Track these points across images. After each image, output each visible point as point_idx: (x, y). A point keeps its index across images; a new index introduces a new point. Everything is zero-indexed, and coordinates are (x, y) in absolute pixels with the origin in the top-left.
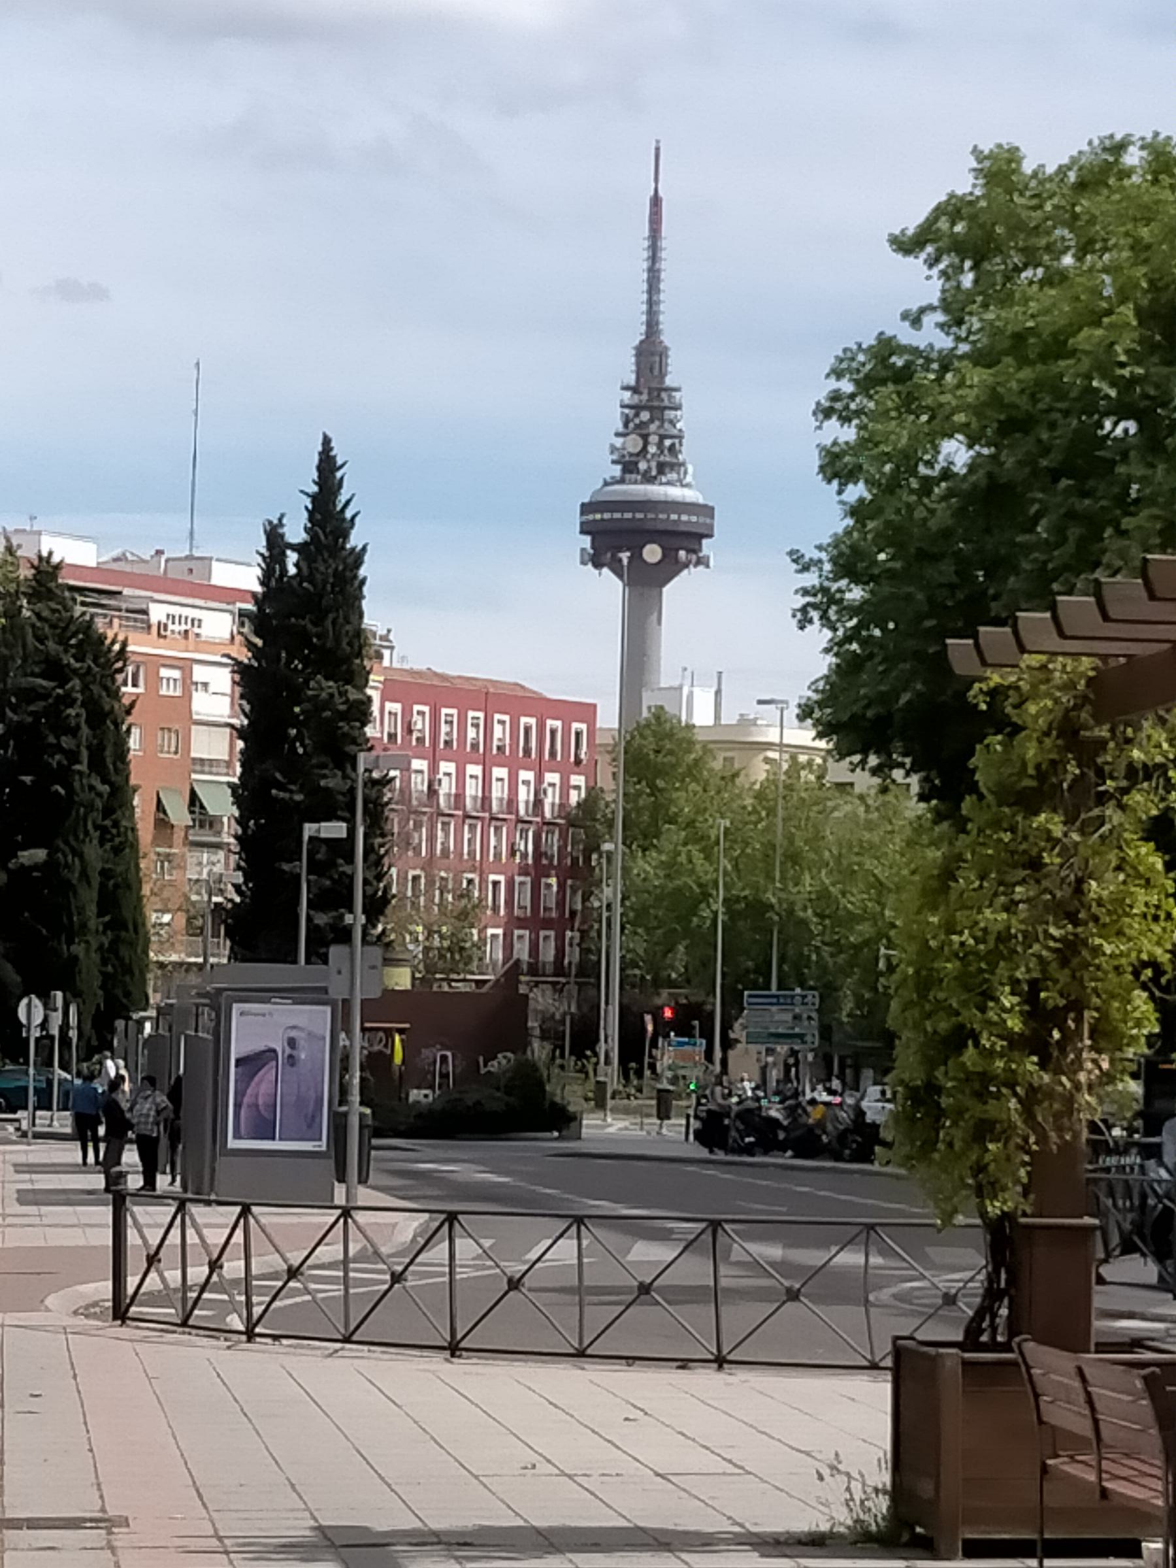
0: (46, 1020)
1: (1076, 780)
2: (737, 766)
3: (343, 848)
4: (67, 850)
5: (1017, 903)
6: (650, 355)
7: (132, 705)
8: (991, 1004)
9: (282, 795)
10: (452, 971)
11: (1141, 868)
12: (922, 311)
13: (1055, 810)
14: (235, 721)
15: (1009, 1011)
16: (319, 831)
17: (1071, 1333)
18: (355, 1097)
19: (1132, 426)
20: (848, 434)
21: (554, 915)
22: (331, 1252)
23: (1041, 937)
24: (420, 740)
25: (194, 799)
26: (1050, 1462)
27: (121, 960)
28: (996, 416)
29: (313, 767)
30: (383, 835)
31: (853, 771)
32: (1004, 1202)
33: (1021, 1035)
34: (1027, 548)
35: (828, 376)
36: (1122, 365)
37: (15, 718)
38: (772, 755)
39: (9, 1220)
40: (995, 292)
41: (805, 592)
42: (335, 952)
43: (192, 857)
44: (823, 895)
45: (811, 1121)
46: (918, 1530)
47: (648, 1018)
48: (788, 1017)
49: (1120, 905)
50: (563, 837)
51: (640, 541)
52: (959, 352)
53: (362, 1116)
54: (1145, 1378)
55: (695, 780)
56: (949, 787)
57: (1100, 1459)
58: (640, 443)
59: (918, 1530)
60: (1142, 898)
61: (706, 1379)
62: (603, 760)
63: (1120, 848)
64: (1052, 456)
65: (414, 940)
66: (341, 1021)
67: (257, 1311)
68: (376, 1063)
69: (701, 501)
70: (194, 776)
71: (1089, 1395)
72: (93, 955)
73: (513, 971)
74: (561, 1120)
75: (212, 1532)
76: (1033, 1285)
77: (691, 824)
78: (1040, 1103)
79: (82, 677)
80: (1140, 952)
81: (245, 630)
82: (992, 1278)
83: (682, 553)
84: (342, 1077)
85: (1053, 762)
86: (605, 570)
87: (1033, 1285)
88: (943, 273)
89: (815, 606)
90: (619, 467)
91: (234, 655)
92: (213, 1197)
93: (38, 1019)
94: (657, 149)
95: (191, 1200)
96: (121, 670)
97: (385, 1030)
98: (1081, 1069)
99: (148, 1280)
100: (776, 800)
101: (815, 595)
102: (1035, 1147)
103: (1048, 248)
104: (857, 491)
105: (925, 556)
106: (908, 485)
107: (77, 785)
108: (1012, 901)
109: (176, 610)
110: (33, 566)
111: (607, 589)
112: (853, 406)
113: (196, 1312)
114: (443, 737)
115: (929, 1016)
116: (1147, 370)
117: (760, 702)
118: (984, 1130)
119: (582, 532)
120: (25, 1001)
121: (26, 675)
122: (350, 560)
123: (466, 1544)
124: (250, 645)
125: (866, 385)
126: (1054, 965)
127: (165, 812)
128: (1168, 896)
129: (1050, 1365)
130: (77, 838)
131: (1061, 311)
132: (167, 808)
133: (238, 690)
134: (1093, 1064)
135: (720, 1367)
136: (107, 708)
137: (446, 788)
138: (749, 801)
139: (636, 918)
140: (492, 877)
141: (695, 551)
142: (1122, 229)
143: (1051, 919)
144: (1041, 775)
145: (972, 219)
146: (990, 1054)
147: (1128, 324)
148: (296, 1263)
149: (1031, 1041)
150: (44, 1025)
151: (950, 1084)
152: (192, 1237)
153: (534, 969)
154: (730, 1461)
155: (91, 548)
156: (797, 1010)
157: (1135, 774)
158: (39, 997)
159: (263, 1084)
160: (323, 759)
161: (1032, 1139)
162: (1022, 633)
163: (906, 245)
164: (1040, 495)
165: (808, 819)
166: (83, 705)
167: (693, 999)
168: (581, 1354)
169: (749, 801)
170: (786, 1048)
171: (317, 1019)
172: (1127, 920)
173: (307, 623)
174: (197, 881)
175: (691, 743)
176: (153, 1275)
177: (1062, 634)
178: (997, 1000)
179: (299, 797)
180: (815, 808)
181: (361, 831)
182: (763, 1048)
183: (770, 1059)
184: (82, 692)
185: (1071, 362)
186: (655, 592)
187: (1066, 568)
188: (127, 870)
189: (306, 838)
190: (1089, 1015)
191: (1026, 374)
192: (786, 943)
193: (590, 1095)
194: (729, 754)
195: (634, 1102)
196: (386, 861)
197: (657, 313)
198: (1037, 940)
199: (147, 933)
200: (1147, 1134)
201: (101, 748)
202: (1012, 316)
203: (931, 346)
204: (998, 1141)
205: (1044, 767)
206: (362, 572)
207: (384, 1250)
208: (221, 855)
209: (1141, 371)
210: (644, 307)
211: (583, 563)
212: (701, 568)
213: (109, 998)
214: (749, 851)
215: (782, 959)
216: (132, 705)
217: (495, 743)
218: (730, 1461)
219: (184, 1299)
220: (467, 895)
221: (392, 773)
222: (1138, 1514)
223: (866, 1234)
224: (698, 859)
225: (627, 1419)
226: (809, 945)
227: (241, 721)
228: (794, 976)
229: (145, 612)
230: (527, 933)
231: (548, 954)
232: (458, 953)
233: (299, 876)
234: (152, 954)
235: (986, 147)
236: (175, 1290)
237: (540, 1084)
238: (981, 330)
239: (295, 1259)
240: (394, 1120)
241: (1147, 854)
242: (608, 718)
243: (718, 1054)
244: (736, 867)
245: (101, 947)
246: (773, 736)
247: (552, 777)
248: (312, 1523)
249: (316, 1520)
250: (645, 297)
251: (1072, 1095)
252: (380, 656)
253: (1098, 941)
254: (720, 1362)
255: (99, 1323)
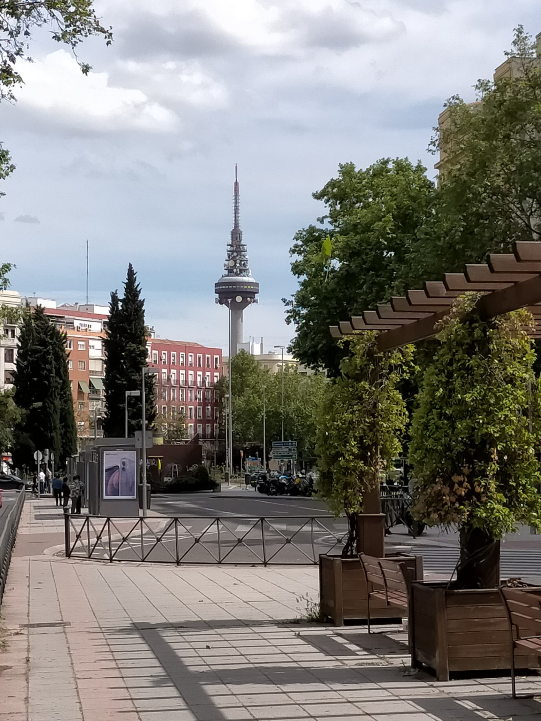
0: (43, 458)
1: (373, 370)
2: (268, 368)
3: (139, 399)
4: (49, 402)
5: (355, 411)
6: (236, 234)
7: (69, 354)
8: (348, 444)
9: (119, 382)
10: (177, 438)
11: (395, 398)
12: (324, 218)
13: (366, 381)
14: (103, 358)
15: (353, 447)
16: (131, 393)
17: (377, 552)
18: (145, 481)
19: (393, 253)
20: (300, 258)
21: (210, 419)
22: (137, 532)
23: (363, 422)
24: (164, 363)
25: (91, 384)
26: (371, 593)
27: (68, 438)
28: (348, 251)
29: (129, 372)
30: (153, 394)
31: (305, 368)
32: (355, 508)
33: (357, 454)
34: (359, 295)
35: (293, 239)
36: (389, 234)
37: (31, 359)
38: (280, 364)
39: (32, 525)
40: (347, 211)
41: (288, 312)
42: (137, 433)
43: (91, 403)
44: (298, 409)
45: (295, 483)
46: (329, 617)
47: (241, 451)
48: (287, 449)
49: (388, 411)
50: (212, 393)
51: (234, 295)
52: (336, 231)
53: (147, 487)
54: (400, 565)
55: (255, 372)
56: (334, 373)
57: (387, 591)
58: (234, 263)
59: (329, 617)
60: (395, 408)
61: (260, 570)
62: (225, 367)
63: (388, 392)
64: (367, 264)
65: (164, 428)
66: (140, 456)
67: (113, 552)
68: (152, 469)
69: (254, 281)
70: (90, 377)
71: (382, 571)
72: (58, 436)
73: (197, 437)
74: (214, 486)
75: (98, 626)
76: (364, 535)
77: (254, 387)
78: (364, 476)
79: (52, 345)
80: (395, 426)
81: (106, 328)
82: (351, 533)
83: (249, 299)
84: (141, 474)
85: (366, 365)
86: (224, 305)
87: (364, 535)
88: (330, 205)
89: (291, 316)
90: (227, 271)
91: (102, 336)
92: (99, 515)
93: (40, 458)
94: (236, 167)
95: (91, 517)
96: (65, 343)
97: (155, 458)
98: (378, 464)
99: (77, 543)
100: (281, 379)
101: (291, 313)
102: (363, 491)
103: (364, 196)
104: (304, 278)
105: (326, 298)
106: (321, 275)
107: (51, 380)
108: (353, 410)
109: (83, 322)
110: (35, 309)
111: (224, 311)
112: (302, 249)
113: (93, 553)
114: (172, 361)
115: (328, 449)
116: (397, 235)
117: (275, 347)
118: (346, 486)
119: (216, 293)
120: (36, 452)
121: (33, 345)
122: (140, 304)
123: (181, 627)
124: (107, 333)
125: (306, 242)
126: (368, 431)
127: (81, 389)
128: (404, 407)
129: (370, 562)
130: (52, 398)
131: (368, 217)
132: (82, 388)
133: (104, 348)
134: (382, 462)
135: (265, 566)
136: (61, 355)
137: (173, 378)
138: (272, 379)
139: (237, 419)
140: (190, 407)
141: (253, 298)
142: (387, 189)
143: (366, 416)
144: (362, 370)
145: (339, 187)
146: (347, 461)
147: (390, 220)
148: (125, 536)
149: (362, 457)
150: (42, 460)
151: (335, 471)
152: (91, 529)
153: (204, 436)
154: (268, 597)
155: (55, 302)
156: (290, 447)
157: (391, 369)
158: (41, 451)
159: (115, 477)
160: (132, 370)
161: (362, 488)
162: (353, 323)
163: (318, 196)
164: (363, 277)
165: (292, 384)
166: (53, 354)
167: (257, 445)
168: (220, 563)
169: (272, 379)
170: (287, 460)
171: (132, 455)
172: (391, 416)
173: (126, 325)
174: (92, 411)
175: (253, 361)
176: (79, 542)
177: (366, 324)
178: (350, 443)
179: (125, 383)
180: (295, 381)
181: (144, 393)
182: (280, 460)
183: (282, 464)
184: (52, 350)
185: (372, 233)
186: (240, 311)
187: (373, 300)
188: (69, 408)
189: (127, 396)
190: (380, 447)
191: (358, 237)
192: (286, 425)
193: (224, 477)
194: (265, 364)
195: (238, 479)
196: (154, 402)
197: (238, 220)
198: (362, 423)
199: (76, 429)
200: (405, 485)
201: (59, 368)
202: (352, 219)
203: (327, 229)
204: (351, 489)
205: (363, 366)
206: (143, 308)
207: (155, 531)
208: (100, 402)
209: (395, 235)
210: (234, 219)
211: (216, 303)
212: (255, 303)
213: (65, 451)
214: (273, 395)
215: (285, 430)
216: (69, 354)
217: (189, 363)
218: (268, 597)
219: (89, 549)
220: (181, 413)
221: (155, 374)
222: (399, 609)
223: (312, 520)
224: (256, 397)
225: (235, 584)
226: (294, 425)
227: (105, 358)
228: (289, 436)
229: (72, 323)
230: (201, 425)
231: (209, 431)
232: (179, 432)
233: (125, 408)
234: (78, 436)
235: (343, 164)
236: (86, 546)
237: (207, 474)
238: (342, 224)
239: (125, 535)
240: (158, 487)
241: (397, 394)
242: (226, 353)
243: (265, 462)
244: (269, 401)
245: (61, 434)
246: (280, 357)
247: (208, 373)
248: (131, 622)
249: (132, 621)
250: (234, 215)
251: (375, 473)
252: (150, 335)
253: (382, 423)
254: (265, 564)
255: (62, 558)
